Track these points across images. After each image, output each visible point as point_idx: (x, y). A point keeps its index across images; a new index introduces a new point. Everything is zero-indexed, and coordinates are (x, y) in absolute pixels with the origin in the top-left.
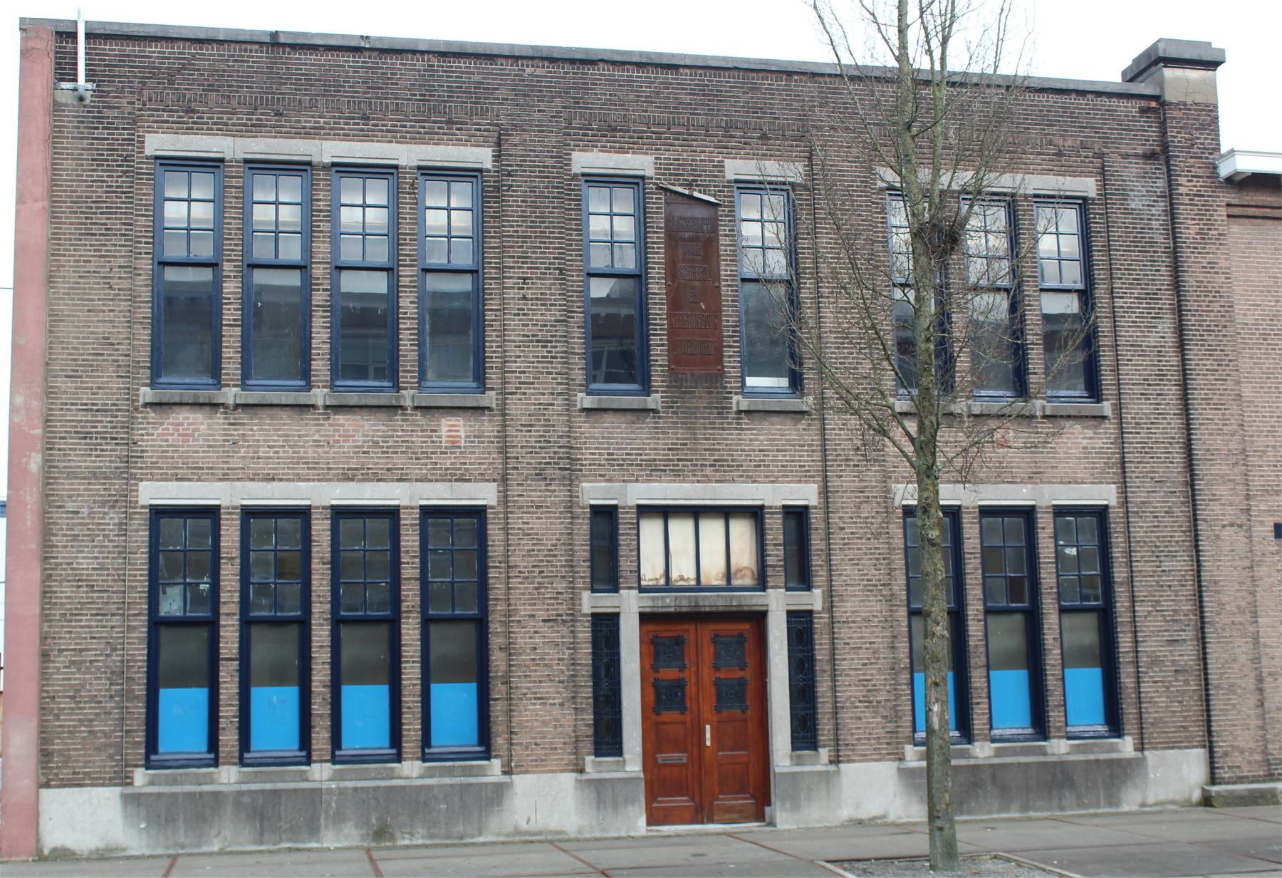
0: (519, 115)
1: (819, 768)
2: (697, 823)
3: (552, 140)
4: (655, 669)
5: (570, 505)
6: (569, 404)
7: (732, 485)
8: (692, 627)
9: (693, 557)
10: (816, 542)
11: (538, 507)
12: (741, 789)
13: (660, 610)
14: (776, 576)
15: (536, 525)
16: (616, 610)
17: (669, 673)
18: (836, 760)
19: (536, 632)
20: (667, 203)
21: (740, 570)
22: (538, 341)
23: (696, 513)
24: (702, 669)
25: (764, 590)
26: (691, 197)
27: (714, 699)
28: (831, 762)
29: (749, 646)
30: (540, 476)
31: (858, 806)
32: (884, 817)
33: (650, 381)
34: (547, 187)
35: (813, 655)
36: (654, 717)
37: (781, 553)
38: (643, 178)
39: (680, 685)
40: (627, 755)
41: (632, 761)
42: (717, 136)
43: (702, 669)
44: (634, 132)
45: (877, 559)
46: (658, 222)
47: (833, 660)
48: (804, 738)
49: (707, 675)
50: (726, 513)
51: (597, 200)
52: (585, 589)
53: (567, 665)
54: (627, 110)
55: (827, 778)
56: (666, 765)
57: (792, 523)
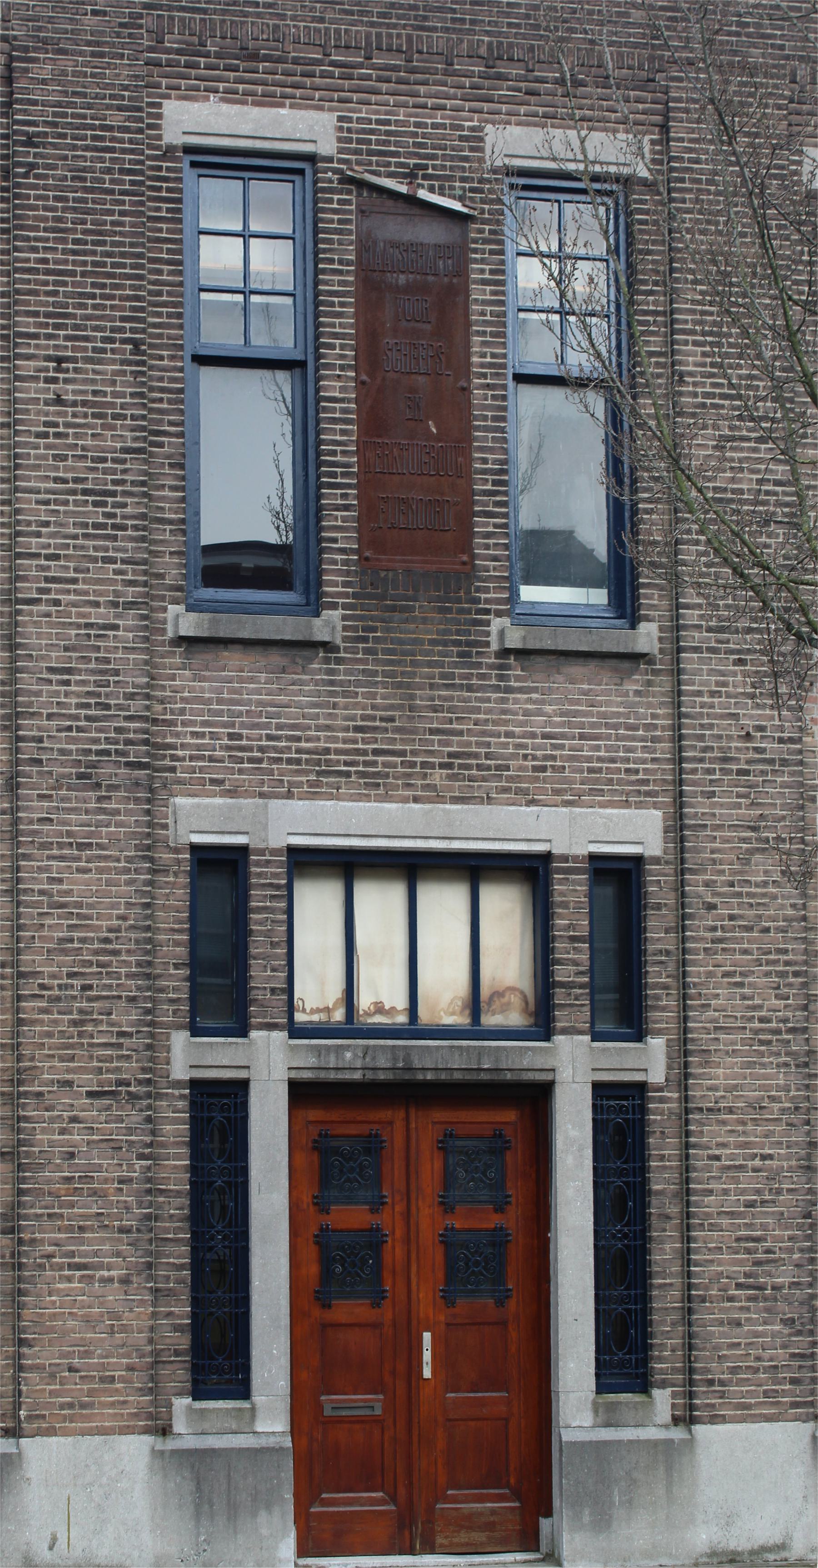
0: (50, 20)
1: (651, 1433)
2: (401, 1553)
3: (122, 72)
4: (322, 1206)
5: (150, 843)
6: (151, 628)
7: (485, 809)
8: (398, 1116)
9: (401, 960)
10: (658, 935)
11: (81, 847)
12: (491, 1478)
13: (332, 1076)
14: (573, 1009)
15: (78, 885)
16: (242, 1074)
17: (351, 1216)
18: (686, 1418)
19: (74, 1120)
20: (361, 212)
21: (497, 994)
22: (85, 492)
23: (413, 867)
24: (419, 1208)
25: (547, 1039)
26: (411, 200)
27: (440, 1275)
28: (676, 1421)
29: (515, 1159)
30: (87, 779)
31: (729, 1520)
32: (782, 1547)
33: (320, 583)
34: (109, 171)
35: (645, 1182)
36: (317, 1312)
37: (585, 957)
38: (311, 158)
39: (373, 1240)
40: (258, 1398)
41: (270, 1411)
42: (471, 75)
43: (418, 1215)
44: (296, 61)
45: (782, 975)
46: (345, 251)
47: (685, 1193)
48: (622, 1364)
49: (429, 1221)
50: (473, 869)
51: (215, 201)
52: (179, 1027)
53: (138, 1194)
54: (283, 17)
55: (669, 1457)
56: (340, 1420)
57: (608, 892)
